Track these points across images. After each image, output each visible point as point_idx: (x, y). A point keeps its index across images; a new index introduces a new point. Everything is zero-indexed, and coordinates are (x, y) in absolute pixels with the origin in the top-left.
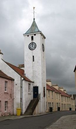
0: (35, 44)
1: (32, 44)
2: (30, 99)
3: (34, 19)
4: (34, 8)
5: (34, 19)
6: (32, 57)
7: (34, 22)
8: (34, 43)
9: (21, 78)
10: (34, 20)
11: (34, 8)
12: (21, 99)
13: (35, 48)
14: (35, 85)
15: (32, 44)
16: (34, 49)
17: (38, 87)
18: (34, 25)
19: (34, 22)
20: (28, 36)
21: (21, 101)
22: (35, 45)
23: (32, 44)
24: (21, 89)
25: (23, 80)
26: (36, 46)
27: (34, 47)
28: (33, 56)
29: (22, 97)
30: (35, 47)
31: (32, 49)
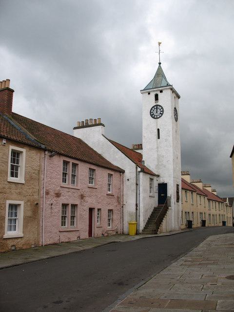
0: (162, 108)
1: (155, 107)
2: (153, 206)
3: (160, 64)
4: (160, 44)
5: (160, 64)
6: (156, 131)
7: (160, 69)
8: (160, 106)
9: (137, 168)
10: (160, 66)
11: (160, 44)
12: (137, 205)
13: (162, 114)
14: (161, 180)
15: (157, 108)
16: (160, 117)
17: (166, 184)
18: (160, 73)
19: (160, 69)
20: (149, 94)
21: (137, 209)
22: (161, 110)
23: (157, 108)
24: (137, 187)
25: (139, 172)
26: (163, 111)
27: (160, 114)
28: (158, 130)
29: (138, 203)
30: (162, 112)
31: (156, 117)
